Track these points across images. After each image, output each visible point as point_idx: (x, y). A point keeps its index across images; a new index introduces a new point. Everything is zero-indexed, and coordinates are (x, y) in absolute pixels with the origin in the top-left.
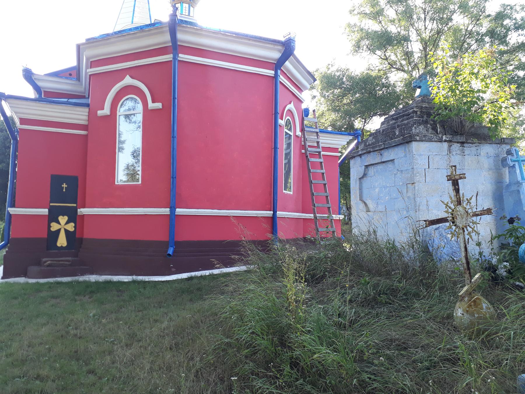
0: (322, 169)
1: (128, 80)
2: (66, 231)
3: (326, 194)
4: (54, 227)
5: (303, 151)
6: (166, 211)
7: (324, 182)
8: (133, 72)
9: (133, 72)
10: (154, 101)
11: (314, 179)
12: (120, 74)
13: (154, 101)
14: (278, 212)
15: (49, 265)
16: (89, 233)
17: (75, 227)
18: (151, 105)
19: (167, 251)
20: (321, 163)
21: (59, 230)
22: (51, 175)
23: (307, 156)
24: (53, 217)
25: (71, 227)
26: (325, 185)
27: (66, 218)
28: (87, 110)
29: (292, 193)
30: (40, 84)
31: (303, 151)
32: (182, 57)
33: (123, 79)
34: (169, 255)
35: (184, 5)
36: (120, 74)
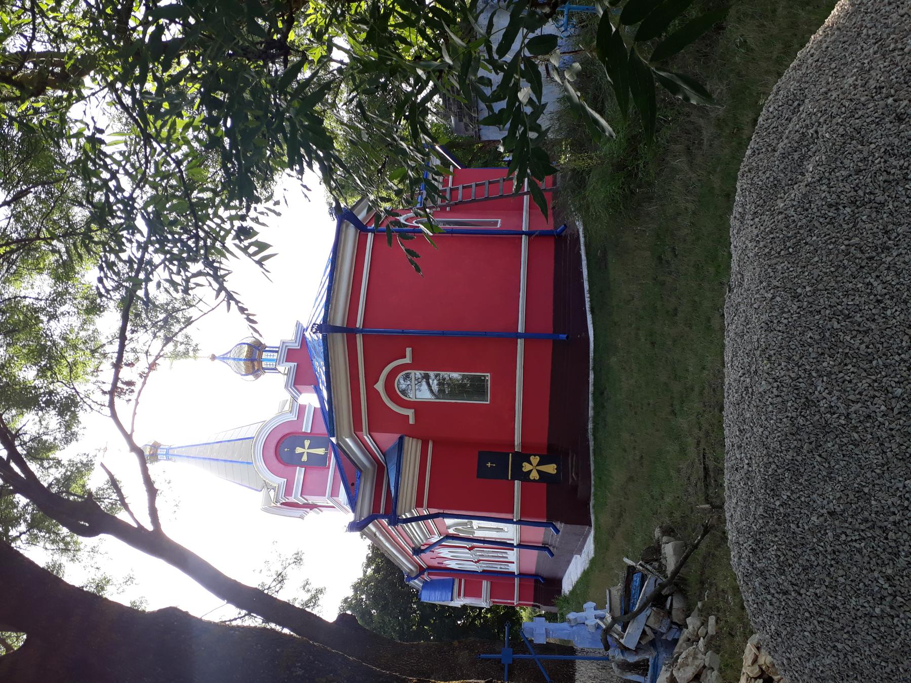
0: (471, 186)
1: (380, 386)
2: (539, 464)
3: (501, 181)
4: (534, 475)
5: (448, 209)
6: (520, 343)
7: (487, 183)
8: (371, 380)
9: (371, 380)
10: (405, 357)
11: (483, 195)
12: (372, 395)
13: (405, 357)
14: (524, 230)
15: (577, 474)
16: (542, 438)
17: (535, 456)
18: (408, 360)
19: (564, 340)
20: (464, 187)
21: (539, 472)
22: (478, 477)
23: (456, 204)
24: (524, 477)
25: (535, 460)
26: (490, 183)
27: (525, 464)
28: (406, 438)
29: (500, 220)
30: (365, 515)
31: (448, 209)
32: (359, 323)
33: (377, 392)
34: (567, 337)
35: (263, 357)
36: (372, 395)
